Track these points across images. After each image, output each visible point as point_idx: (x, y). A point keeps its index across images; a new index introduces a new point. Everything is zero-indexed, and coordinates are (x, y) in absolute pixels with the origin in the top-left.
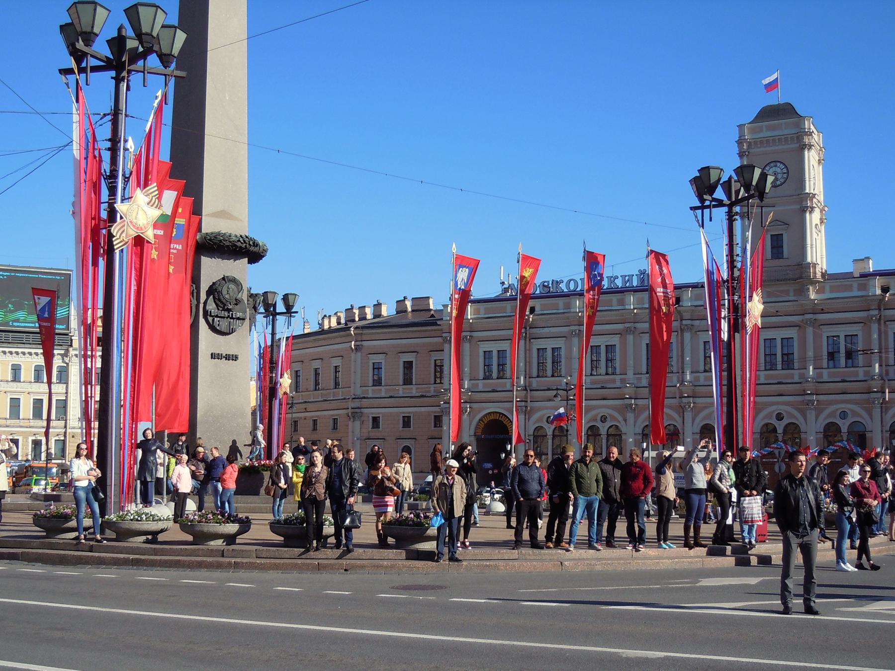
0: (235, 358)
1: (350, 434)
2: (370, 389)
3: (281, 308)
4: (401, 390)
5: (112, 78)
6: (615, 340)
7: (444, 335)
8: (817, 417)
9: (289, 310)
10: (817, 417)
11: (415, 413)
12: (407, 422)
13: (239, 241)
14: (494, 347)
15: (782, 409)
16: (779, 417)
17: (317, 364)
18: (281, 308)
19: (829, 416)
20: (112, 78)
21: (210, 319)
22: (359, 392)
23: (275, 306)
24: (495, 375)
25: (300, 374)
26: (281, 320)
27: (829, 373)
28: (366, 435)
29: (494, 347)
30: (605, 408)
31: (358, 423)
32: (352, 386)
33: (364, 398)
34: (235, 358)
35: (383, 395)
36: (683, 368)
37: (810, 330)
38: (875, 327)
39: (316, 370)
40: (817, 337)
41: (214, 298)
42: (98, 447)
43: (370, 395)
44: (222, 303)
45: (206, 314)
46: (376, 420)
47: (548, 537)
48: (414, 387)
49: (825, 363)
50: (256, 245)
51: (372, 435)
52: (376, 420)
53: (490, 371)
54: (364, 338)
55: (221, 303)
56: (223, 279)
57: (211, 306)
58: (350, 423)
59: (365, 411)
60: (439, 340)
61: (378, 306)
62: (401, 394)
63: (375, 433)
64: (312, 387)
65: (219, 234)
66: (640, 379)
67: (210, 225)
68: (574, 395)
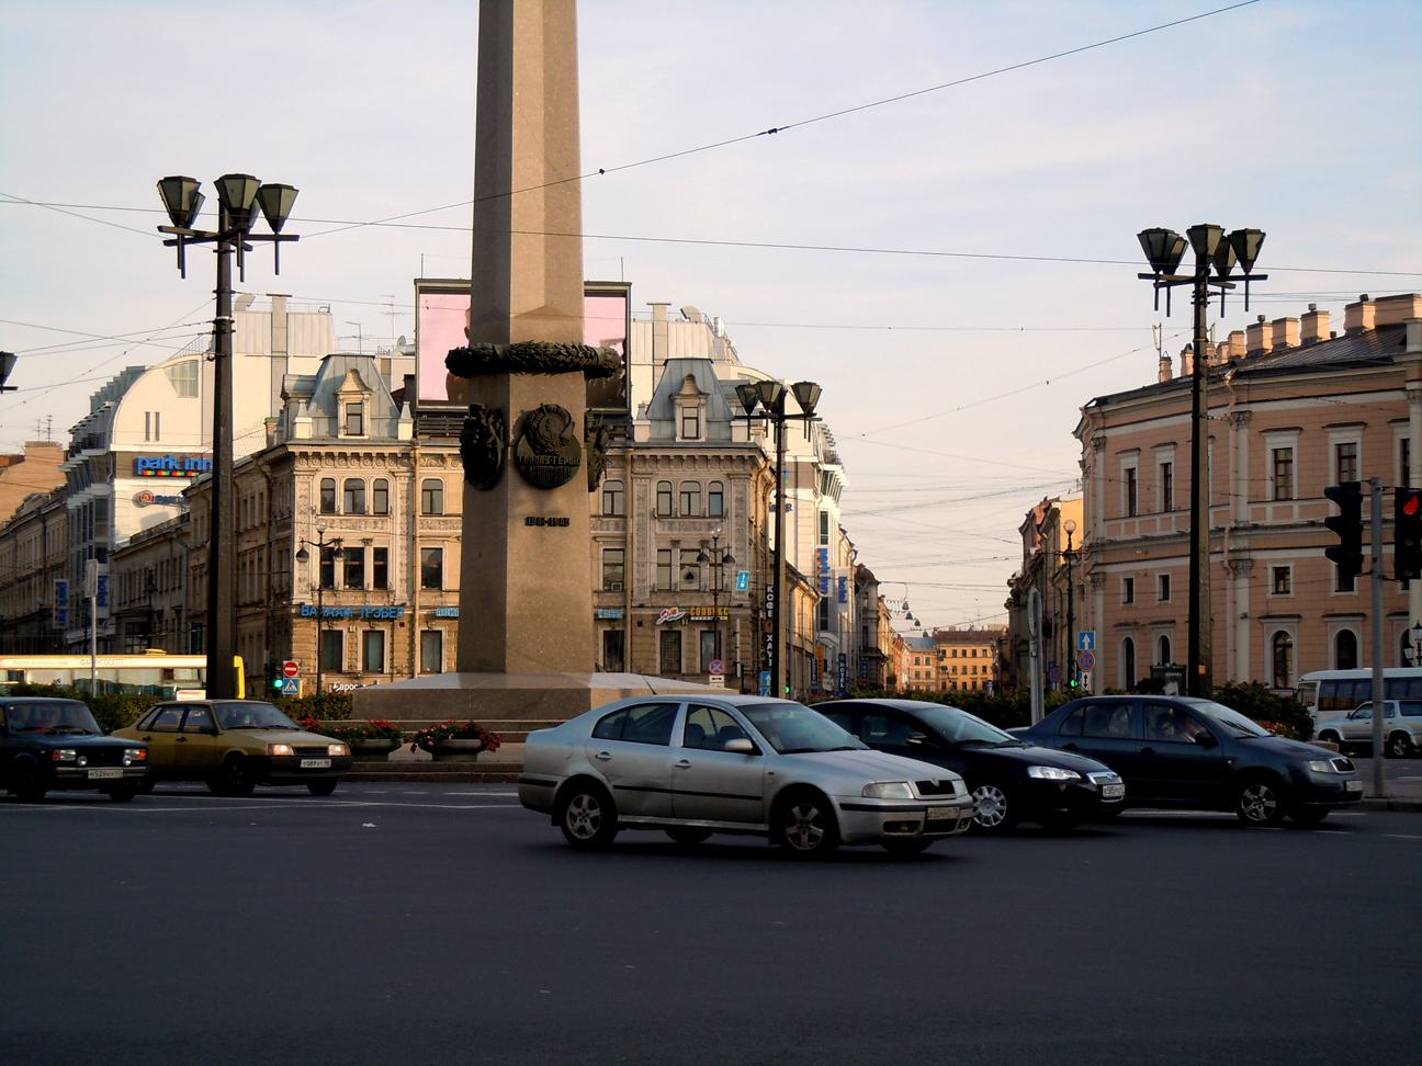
1: (1229, 606)
2: (1269, 508)
3: (792, 406)
5: (215, 251)
7: (1410, 386)
9: (808, 414)
11: (1297, 560)
13: (560, 353)
17: (1130, 461)
20: (215, 251)
21: (523, 468)
22: (1246, 514)
25: (1173, 471)
26: (794, 429)
27: (1291, 516)
28: (1262, 609)
31: (1243, 583)
33: (1256, 527)
35: (1296, 519)
39: (1166, 466)
40: (1255, 451)
41: (528, 439)
42: (1206, 810)
43: (1269, 521)
44: (540, 444)
45: (519, 464)
46: (1281, 574)
47: (366, 667)
48: (1296, 506)
50: (695, 309)
51: (1276, 609)
53: (1288, 486)
54: (1255, 395)
55: (534, 441)
56: (541, 410)
57: (524, 449)
58: (1229, 584)
59: (1257, 556)
60: (1399, 395)
61: (1311, 316)
63: (1281, 605)
65: (529, 345)
67: (520, 332)
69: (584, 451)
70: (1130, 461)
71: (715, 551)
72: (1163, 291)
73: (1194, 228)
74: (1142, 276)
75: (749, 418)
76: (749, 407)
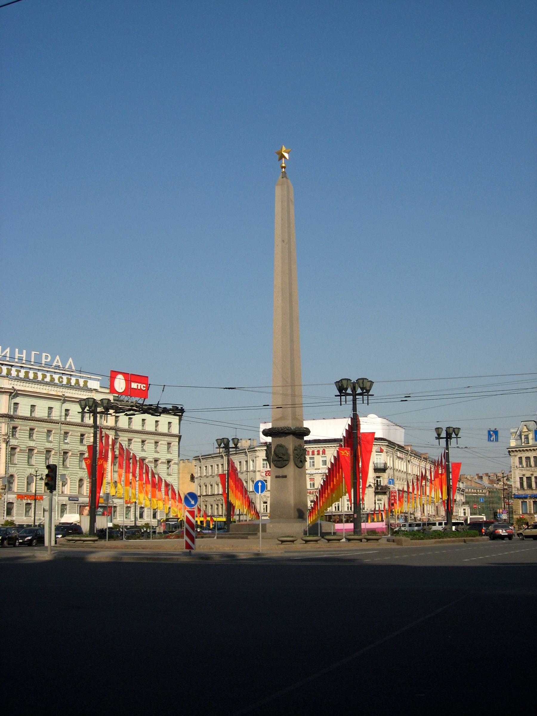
0: (285, 477)
3: (231, 445)
34: (285, 477)
69: (292, 457)
72: (365, 397)
73: (337, 382)
76: (220, 445)
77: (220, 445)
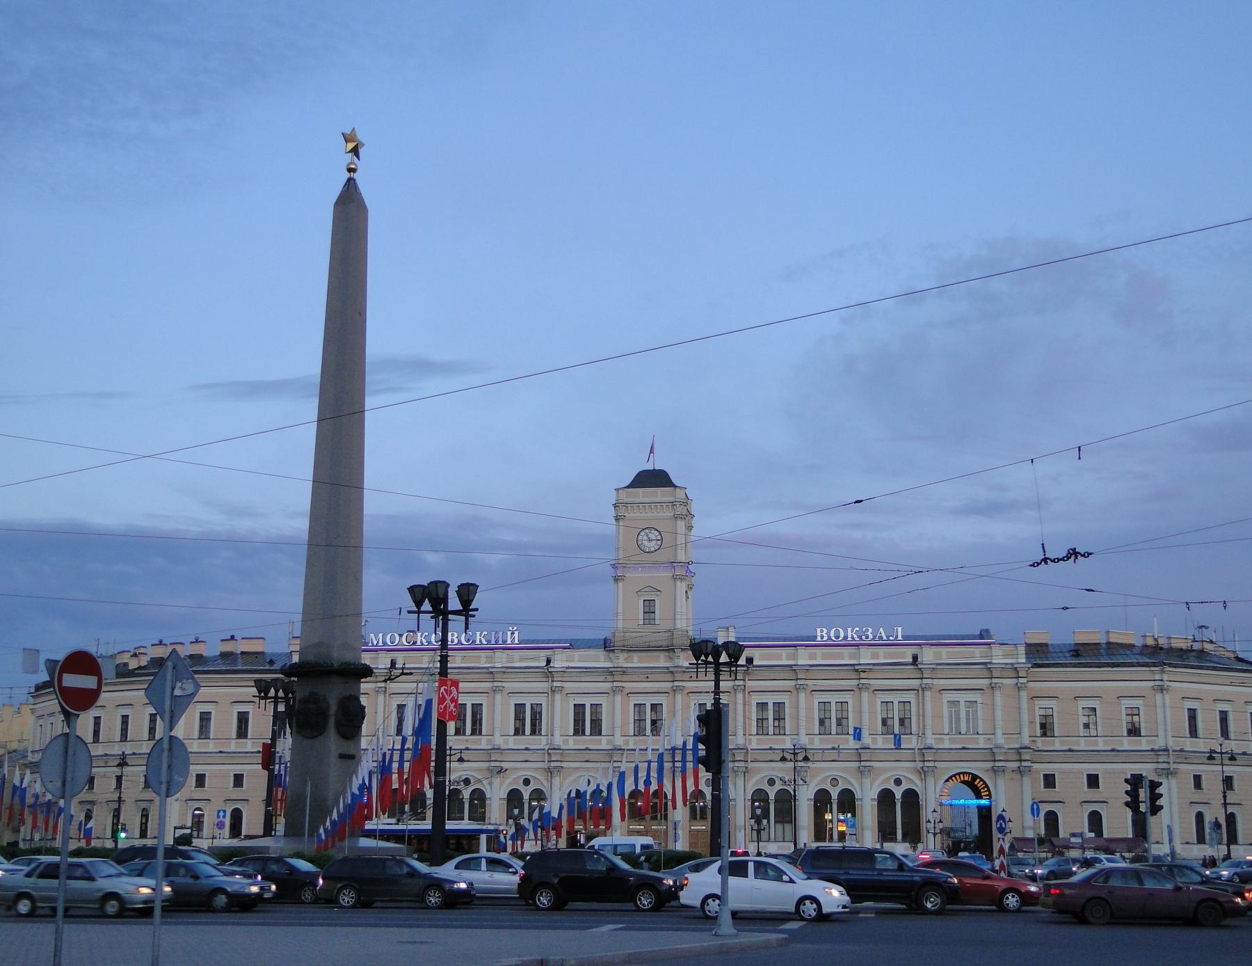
3: (454, 603)
4: (234, 746)
6: (541, 699)
8: (501, 784)
9: (466, 609)
10: (501, 784)
12: (1093, 781)
14: (770, 700)
15: (528, 774)
16: (527, 782)
17: (125, 711)
18: (454, 603)
19: (757, 782)
23: (445, 600)
24: (588, 731)
25: (1231, 717)
26: (456, 623)
29: (963, 697)
30: (835, 769)
32: (1161, 733)
36: (552, 731)
37: (381, 697)
38: (740, 696)
46: (1197, 780)
48: (1144, 740)
49: (1039, 732)
52: (1197, 780)
62: (1126, 747)
64: (118, 738)
66: (942, 739)
68: (800, 756)
70: (125, 711)
71: (706, 663)
74: (409, 612)
75: (419, 612)
77: (418, 604)
